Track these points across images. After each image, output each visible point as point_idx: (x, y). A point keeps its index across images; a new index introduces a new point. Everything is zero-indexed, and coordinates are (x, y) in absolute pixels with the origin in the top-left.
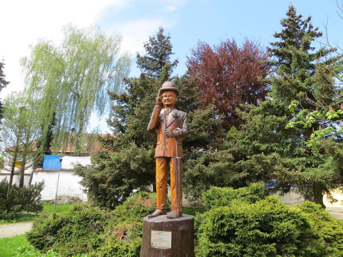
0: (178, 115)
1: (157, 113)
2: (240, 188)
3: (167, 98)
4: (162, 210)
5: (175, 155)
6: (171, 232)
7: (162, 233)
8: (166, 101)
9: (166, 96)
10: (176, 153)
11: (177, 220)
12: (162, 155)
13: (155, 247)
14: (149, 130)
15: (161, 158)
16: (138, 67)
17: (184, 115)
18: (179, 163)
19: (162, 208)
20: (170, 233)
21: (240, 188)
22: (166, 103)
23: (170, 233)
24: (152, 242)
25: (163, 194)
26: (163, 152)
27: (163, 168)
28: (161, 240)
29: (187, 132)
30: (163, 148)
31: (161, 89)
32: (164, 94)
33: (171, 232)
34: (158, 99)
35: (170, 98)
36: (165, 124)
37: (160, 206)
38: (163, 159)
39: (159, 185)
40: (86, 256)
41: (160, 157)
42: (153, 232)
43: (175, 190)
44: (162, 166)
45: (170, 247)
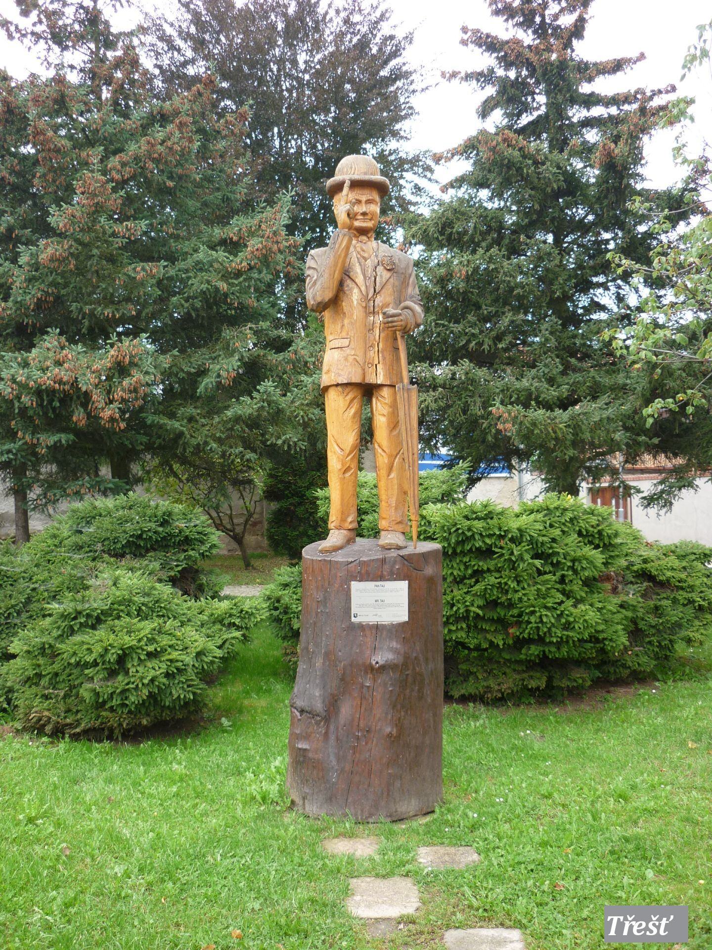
20: (404, 585)
23: (404, 585)
26: (360, 371)
45: (406, 619)
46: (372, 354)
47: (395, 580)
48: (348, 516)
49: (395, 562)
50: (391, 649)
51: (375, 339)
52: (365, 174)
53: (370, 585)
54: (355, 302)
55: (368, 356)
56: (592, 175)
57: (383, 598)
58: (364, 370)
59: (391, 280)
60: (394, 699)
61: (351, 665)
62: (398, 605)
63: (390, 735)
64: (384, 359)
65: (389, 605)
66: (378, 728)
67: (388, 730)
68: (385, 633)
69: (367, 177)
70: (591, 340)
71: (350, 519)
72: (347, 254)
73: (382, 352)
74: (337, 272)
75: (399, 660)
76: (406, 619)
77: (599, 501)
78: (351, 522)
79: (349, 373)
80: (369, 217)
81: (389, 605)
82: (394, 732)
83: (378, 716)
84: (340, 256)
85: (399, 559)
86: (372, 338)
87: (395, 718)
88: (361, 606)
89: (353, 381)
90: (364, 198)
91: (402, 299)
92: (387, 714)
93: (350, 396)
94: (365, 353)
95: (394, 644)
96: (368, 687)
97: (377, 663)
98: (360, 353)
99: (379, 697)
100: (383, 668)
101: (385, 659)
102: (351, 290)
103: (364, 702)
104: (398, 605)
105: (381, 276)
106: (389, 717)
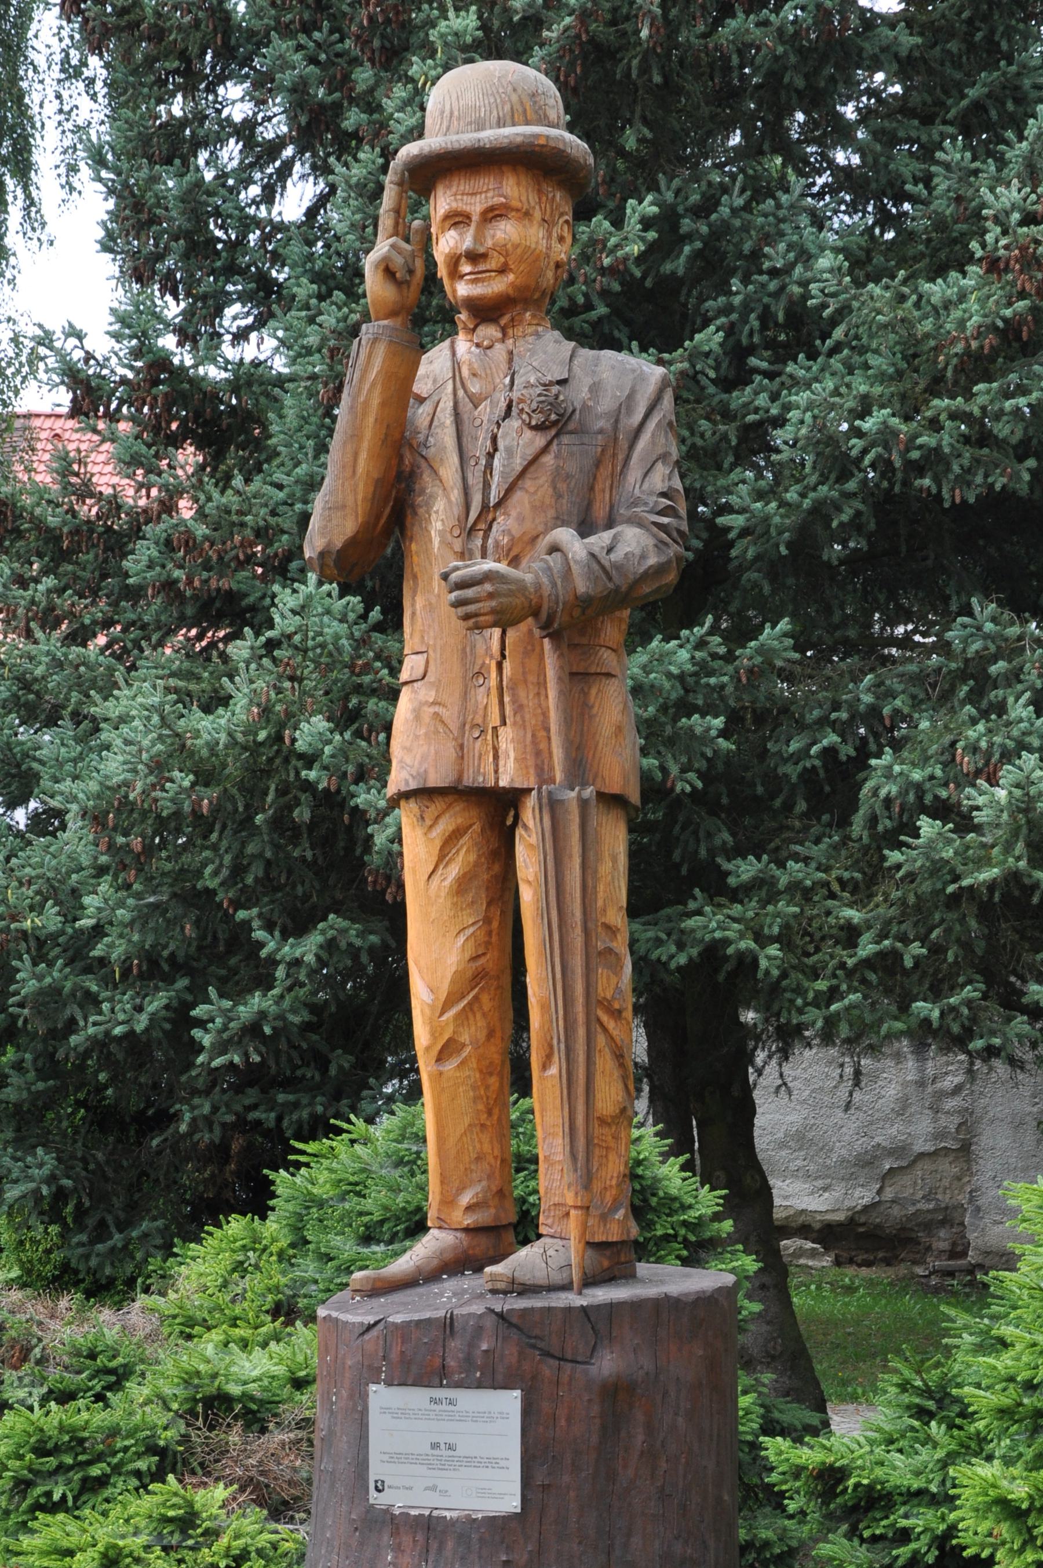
0: (579, 394)
1: (375, 402)
2: (281, 1177)
3: (467, 243)
4: (467, 1230)
5: (544, 776)
6: (517, 1393)
8: (466, 268)
9: (457, 219)
11: (601, 1295)
13: (414, 1512)
14: (322, 555)
15: (439, 804)
16: (103, 224)
17: (631, 397)
19: (468, 1221)
20: (511, 1401)
21: (281, 1177)
23: (511, 1401)
25: (475, 1099)
26: (450, 751)
27: (461, 886)
28: (444, 1452)
29: (652, 560)
30: (450, 714)
31: (410, 150)
34: (377, 266)
35: (505, 231)
36: (456, 495)
37: (448, 1202)
38: (458, 807)
39: (434, 1035)
41: (424, 794)
43: (553, 1070)
44: (453, 871)
45: (512, 1504)
46: (485, 697)
48: (461, 1190)
52: (480, 126)
53: (417, 1397)
54: (436, 541)
55: (470, 706)
56: (602, 310)
57: (450, 1440)
59: (548, 459)
62: (492, 1463)
65: (470, 1461)
68: (450, 1544)
69: (491, 136)
73: (513, 689)
74: (363, 456)
76: (512, 1504)
78: (469, 1208)
80: (493, 263)
81: (470, 1461)
84: (366, 403)
85: (490, 1322)
86: (481, 648)
88: (395, 1458)
89: (432, 783)
91: (600, 512)
93: (445, 826)
94: (465, 695)
98: (452, 698)
102: (433, 497)
104: (492, 1463)
105: (510, 452)
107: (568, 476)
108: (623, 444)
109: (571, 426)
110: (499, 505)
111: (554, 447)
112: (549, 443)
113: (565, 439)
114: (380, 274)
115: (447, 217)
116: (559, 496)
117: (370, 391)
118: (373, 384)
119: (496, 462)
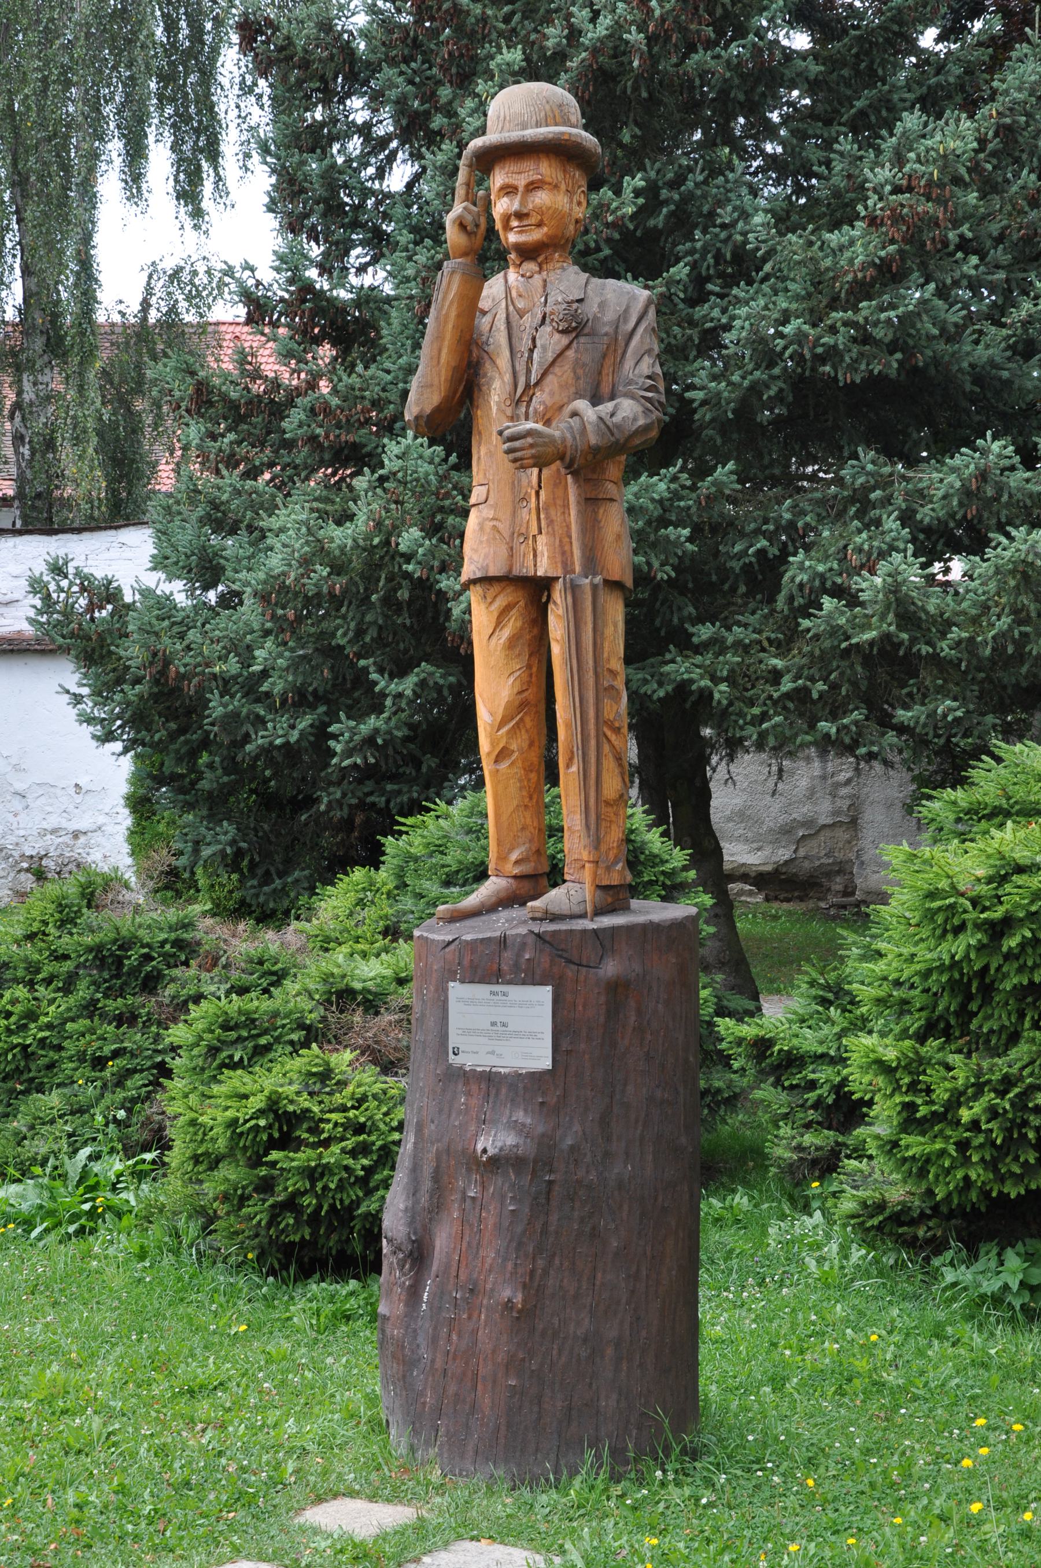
0: (591, 308)
1: (453, 314)
3: (516, 206)
4: (515, 877)
6: (549, 988)
7: (505, 994)
8: (515, 223)
10: (573, 563)
12: (495, 570)
13: (479, 1069)
15: (496, 588)
16: (268, 193)
18: (556, 649)
19: (516, 871)
20: (544, 994)
22: (512, 238)
23: (544, 994)
24: (454, 1040)
26: (503, 551)
27: (512, 643)
30: (504, 527)
32: (499, 178)
33: (549, 988)
34: (454, 222)
35: (541, 198)
38: (509, 590)
39: (493, 744)
40: (2, 173)
41: (485, 580)
42: (456, 990)
43: (574, 769)
44: (506, 633)
47: (524, 983)
48: (511, 850)
49: (523, 946)
50: (515, 1126)
51: (530, 482)
53: (481, 991)
55: (518, 521)
58: (512, 548)
59: (571, 353)
60: (519, 1229)
61: (448, 1151)
62: (532, 1035)
63: (509, 1305)
64: (551, 523)
65: (518, 1034)
66: (489, 1286)
67: (507, 1293)
68: (504, 1091)
69: (533, 133)
70: (1020, 1360)
71: (514, 856)
72: (544, 375)
73: (546, 509)
75: (527, 1148)
76: (546, 1063)
77: (901, 653)
78: (517, 862)
79: (486, 556)
81: (518, 1034)
82: (518, 1299)
83: (489, 1261)
84: (447, 315)
85: (531, 940)
87: (520, 1270)
88: (467, 1032)
89: (491, 574)
90: (521, 181)
92: (505, 1259)
94: (514, 514)
95: (520, 1116)
96: (473, 1198)
97: (485, 1151)
98: (505, 515)
99: (491, 1222)
100: (496, 1163)
101: (499, 1144)
102: (492, 379)
103: (467, 1227)
104: (532, 1035)
106: (510, 1266)
107: (584, 365)
108: (621, 342)
109: (586, 331)
110: (537, 384)
111: (575, 345)
112: (571, 342)
113: (582, 339)
114: (456, 227)
115: (502, 189)
116: (578, 378)
117: (449, 307)
118: (452, 302)
119: (535, 355)
